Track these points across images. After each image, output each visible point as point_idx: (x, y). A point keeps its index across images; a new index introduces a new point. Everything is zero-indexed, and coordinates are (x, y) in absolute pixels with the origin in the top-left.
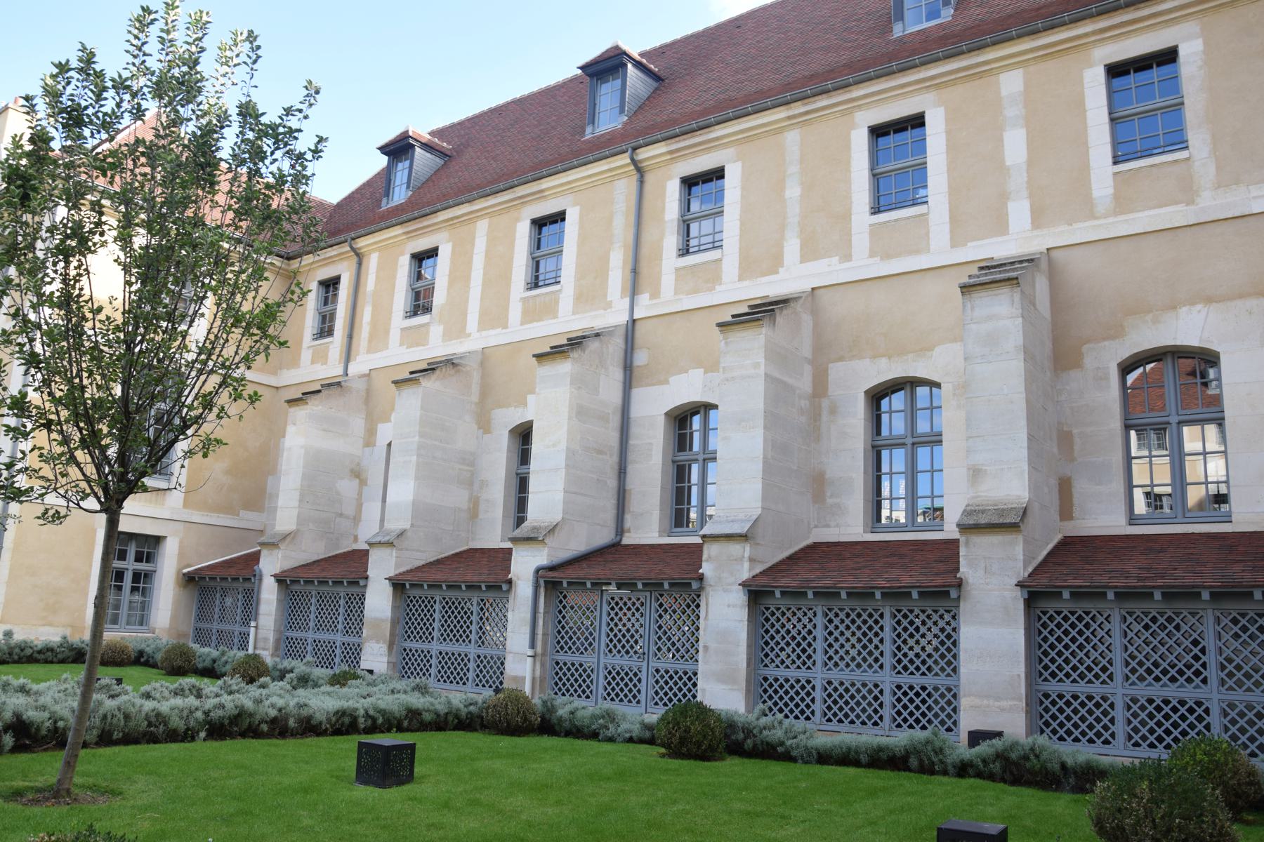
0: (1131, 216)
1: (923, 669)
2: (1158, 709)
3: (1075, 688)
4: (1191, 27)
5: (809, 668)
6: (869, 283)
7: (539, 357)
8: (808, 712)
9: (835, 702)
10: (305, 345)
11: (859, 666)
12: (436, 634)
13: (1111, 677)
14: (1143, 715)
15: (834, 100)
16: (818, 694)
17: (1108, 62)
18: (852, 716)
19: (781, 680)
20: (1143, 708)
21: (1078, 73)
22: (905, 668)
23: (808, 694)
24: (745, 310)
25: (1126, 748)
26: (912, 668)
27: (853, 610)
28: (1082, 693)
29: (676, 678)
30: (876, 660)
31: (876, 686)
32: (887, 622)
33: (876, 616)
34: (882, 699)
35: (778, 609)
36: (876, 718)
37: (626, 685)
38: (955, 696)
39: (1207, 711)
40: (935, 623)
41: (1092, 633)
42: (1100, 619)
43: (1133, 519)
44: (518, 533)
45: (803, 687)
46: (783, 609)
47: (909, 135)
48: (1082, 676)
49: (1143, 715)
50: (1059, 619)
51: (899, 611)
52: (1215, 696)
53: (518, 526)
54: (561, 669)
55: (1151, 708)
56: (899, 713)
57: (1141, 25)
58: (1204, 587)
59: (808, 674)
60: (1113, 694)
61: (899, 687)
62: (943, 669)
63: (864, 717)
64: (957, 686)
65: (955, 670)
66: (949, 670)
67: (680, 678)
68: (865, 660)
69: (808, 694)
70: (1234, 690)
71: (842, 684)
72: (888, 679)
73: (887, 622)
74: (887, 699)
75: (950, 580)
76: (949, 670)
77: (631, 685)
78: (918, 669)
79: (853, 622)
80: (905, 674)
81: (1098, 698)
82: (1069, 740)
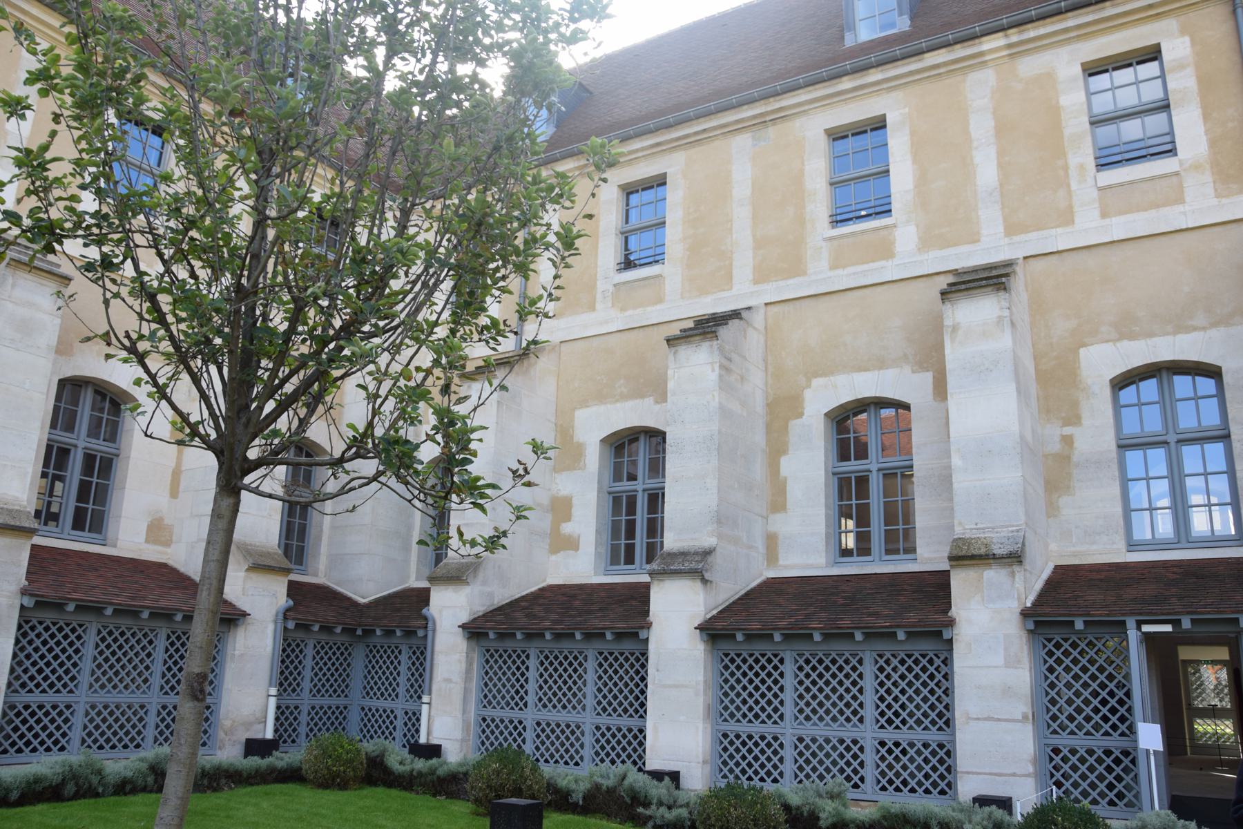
0: (1045, 233)
1: (750, 716)
2: (1082, 760)
3: (43, 698)
4: (1171, 24)
5: (71, 691)
6: (1162, 238)
7: (671, 341)
8: (776, 774)
9: (808, 762)
10: (601, 285)
11: (834, 719)
12: (401, 690)
13: (781, 717)
14: (1101, 769)
15: (1042, 31)
16: (788, 753)
17: (1084, 61)
18: (913, 783)
19: (769, 738)
20: (834, 748)
21: (1057, 66)
22: (890, 722)
23: (855, 757)
24: (691, 324)
25: (875, 793)
26: (763, 716)
27: (827, 655)
28: (757, 733)
29: (619, 736)
30: (855, 713)
31: (142, 707)
32: (868, 669)
33: (776, 661)
34: (862, 757)
35: (751, 655)
36: (943, 785)
37: (624, 749)
38: (948, 753)
39: (861, 749)
40: (894, 669)
41: (1057, 678)
42: (937, 662)
43: (1132, 546)
44: (440, 570)
45: (848, 749)
46: (745, 655)
47: (869, 139)
48: (757, 716)
49: (1101, 769)
50: (924, 662)
51: (881, 656)
52: (155, 700)
53: (436, 565)
54: (543, 731)
55: (1109, 761)
56: (883, 774)
57: (1116, 23)
58: (898, 627)
59: (775, 730)
60: (783, 734)
61: (883, 744)
62: (933, 723)
63: (927, 784)
64: (953, 742)
65: (947, 723)
66: (941, 723)
67: (624, 736)
68: (814, 711)
69: (855, 757)
70: (1110, 735)
71: (609, 729)
72: (869, 734)
73: (868, 669)
74: (869, 757)
75: (942, 618)
76: (941, 723)
77: (618, 749)
78: (744, 716)
79: (827, 669)
80: (890, 729)
81: (1065, 751)
82: (906, 790)
